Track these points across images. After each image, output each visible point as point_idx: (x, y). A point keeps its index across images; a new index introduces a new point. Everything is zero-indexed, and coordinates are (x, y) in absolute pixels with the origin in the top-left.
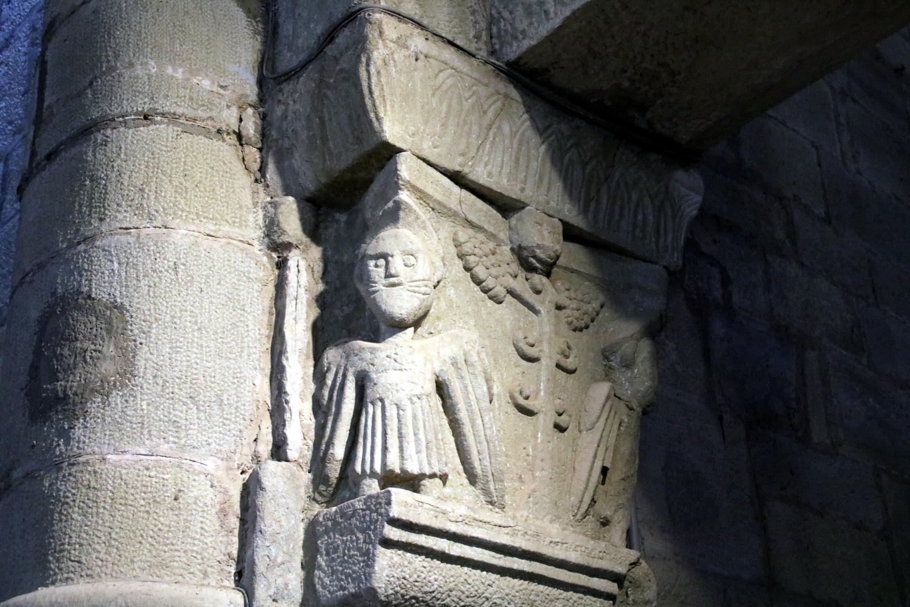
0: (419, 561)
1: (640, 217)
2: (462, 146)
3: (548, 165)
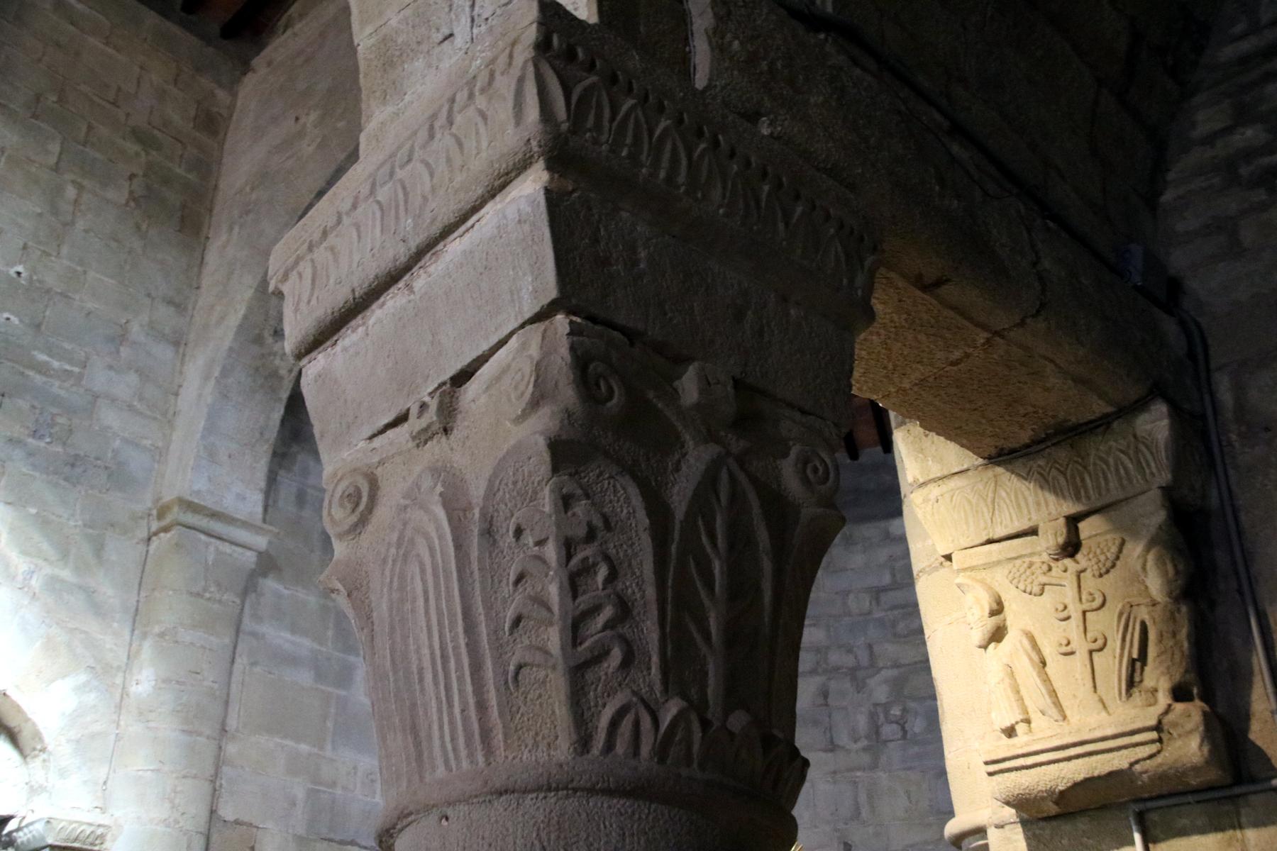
0: (1013, 774)
1: (1122, 471)
2: (982, 525)
3: (1039, 491)
